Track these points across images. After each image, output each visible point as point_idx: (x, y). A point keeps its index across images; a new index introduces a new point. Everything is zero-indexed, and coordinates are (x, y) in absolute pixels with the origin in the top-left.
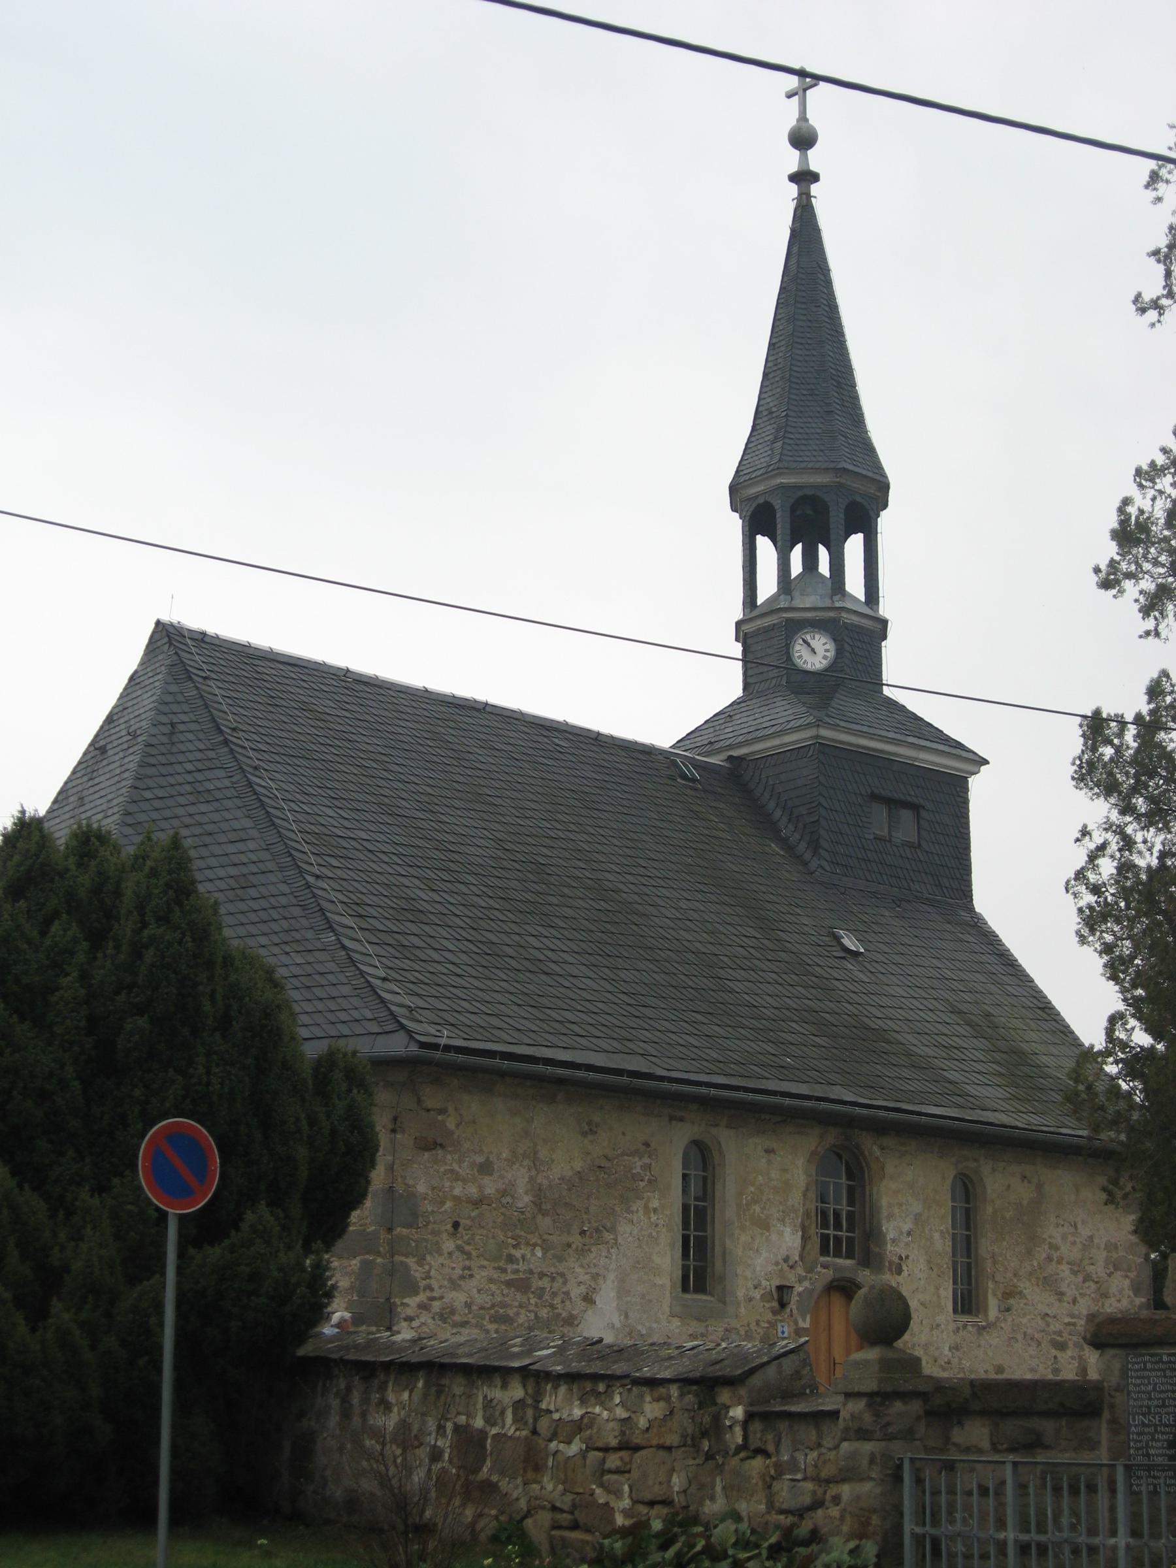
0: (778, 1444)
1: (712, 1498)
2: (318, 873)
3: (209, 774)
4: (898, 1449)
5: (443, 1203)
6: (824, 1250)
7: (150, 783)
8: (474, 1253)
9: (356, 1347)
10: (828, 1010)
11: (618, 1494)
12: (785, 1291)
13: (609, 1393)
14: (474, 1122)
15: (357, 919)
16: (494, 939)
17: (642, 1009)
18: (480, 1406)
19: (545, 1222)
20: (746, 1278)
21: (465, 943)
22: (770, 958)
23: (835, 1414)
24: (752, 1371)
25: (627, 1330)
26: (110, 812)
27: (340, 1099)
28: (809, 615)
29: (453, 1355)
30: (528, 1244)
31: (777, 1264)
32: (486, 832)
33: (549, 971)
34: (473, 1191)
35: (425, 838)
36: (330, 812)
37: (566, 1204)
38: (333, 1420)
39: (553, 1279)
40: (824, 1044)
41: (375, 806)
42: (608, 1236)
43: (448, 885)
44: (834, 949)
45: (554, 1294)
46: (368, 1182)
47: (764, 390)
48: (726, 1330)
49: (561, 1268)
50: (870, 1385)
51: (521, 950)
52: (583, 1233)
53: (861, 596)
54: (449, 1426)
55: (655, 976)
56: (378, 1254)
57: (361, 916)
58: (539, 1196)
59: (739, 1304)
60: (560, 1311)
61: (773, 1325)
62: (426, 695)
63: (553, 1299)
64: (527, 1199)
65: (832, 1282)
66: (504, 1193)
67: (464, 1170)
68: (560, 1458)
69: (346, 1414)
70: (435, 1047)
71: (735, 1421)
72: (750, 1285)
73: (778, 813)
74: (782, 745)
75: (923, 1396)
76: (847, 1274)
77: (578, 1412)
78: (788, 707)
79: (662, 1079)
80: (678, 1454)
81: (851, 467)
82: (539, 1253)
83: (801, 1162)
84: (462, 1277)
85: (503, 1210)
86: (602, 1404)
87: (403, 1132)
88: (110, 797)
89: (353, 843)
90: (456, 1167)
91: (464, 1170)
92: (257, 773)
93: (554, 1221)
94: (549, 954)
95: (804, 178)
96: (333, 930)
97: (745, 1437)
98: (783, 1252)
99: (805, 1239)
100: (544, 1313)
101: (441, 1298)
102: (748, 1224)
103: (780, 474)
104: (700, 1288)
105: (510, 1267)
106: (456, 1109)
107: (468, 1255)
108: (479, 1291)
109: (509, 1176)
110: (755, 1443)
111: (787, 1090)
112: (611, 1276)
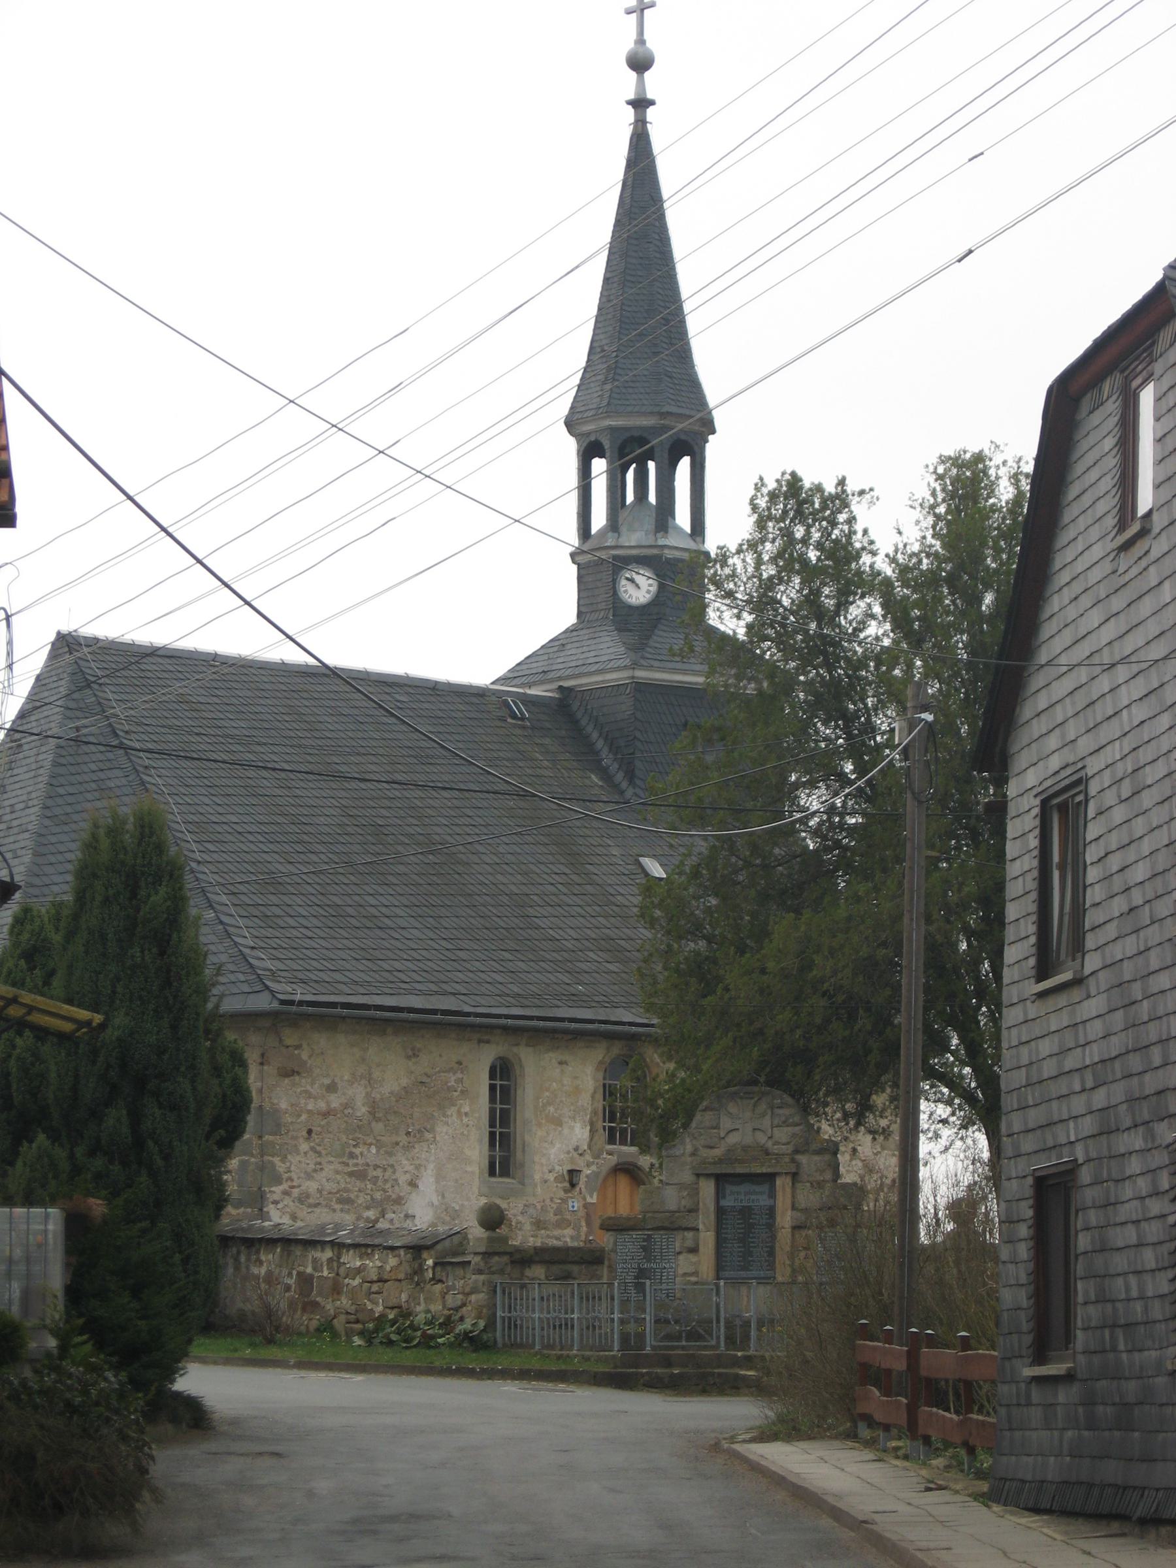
0: (447, 1277)
1: (419, 1304)
2: (200, 859)
3: (110, 774)
4: (497, 1279)
5: (299, 1116)
6: (611, 1140)
7: (62, 780)
8: (324, 1152)
9: (243, 1229)
10: (624, 937)
11: (377, 1304)
12: (575, 1174)
13: (372, 1254)
14: (322, 1053)
15: (231, 897)
16: (339, 902)
17: (458, 952)
18: (310, 1261)
19: (378, 1127)
20: (542, 1165)
21: (315, 907)
22: (576, 892)
23: (469, 1262)
24: (437, 1242)
25: (444, 1207)
26: (30, 803)
27: (227, 1072)
28: (634, 552)
29: (297, 1234)
30: (365, 1144)
31: (568, 1152)
32: (333, 801)
33: (383, 926)
34: (322, 1105)
35: (282, 815)
36: (207, 801)
37: (395, 1112)
38: (230, 1270)
39: (385, 1170)
40: (616, 970)
41: (242, 789)
42: (428, 1136)
43: (302, 856)
44: (638, 876)
45: (386, 1181)
46: (246, 1123)
47: (597, 332)
48: (525, 1206)
49: (391, 1161)
50: (482, 1249)
51: (361, 909)
52: (408, 1133)
53: (687, 528)
54: (295, 1273)
55: (472, 921)
56: (252, 1155)
57: (234, 894)
58: (373, 1107)
59: (536, 1186)
60: (390, 1193)
61: (564, 1201)
62: (283, 668)
63: (385, 1184)
64: (364, 1110)
65: (616, 1165)
66: (346, 1106)
67: (315, 1090)
68: (350, 1287)
69: (237, 1268)
70: (291, 1003)
71: (429, 1266)
72: (545, 1169)
73: (600, 744)
74: (603, 682)
75: (510, 1254)
76: (630, 1160)
77: (358, 1264)
78: (611, 644)
79: (468, 1014)
80: (404, 1283)
81: (674, 409)
82: (373, 1150)
83: (589, 1070)
84: (315, 1171)
85: (346, 1119)
86: (370, 1259)
87: (269, 1064)
88: (30, 789)
89: (226, 827)
90: (309, 1088)
91: (315, 1090)
92: (148, 772)
93: (385, 1126)
94: (384, 910)
95: (641, 104)
96: (212, 908)
97: (434, 1274)
98: (574, 1143)
99: (593, 1132)
100: (378, 1195)
101: (299, 1186)
102: (543, 1121)
103: (609, 417)
104: (505, 1172)
105: (351, 1162)
106: (308, 1044)
107: (319, 1154)
108: (328, 1180)
109: (350, 1092)
110: (438, 1277)
111: (574, 1016)
112: (431, 1166)
